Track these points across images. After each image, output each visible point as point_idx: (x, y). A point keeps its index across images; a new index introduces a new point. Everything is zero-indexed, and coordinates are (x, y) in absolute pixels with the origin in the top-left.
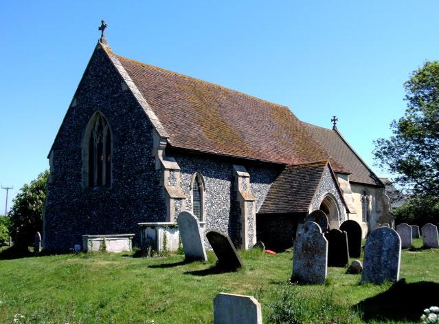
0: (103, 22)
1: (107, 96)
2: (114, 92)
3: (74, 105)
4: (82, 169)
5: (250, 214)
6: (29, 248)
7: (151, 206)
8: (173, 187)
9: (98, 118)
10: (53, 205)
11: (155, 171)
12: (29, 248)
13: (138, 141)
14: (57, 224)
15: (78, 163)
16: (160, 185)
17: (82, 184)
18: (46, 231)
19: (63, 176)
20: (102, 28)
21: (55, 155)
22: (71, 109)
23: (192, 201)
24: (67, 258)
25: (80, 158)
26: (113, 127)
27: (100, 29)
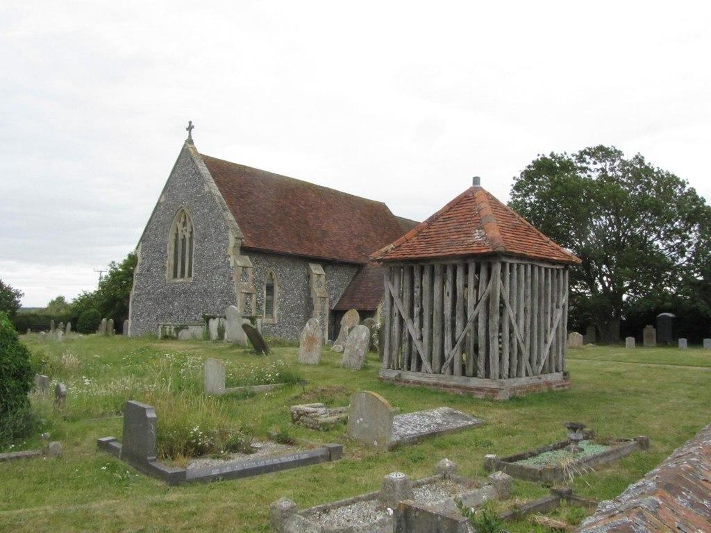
0: (190, 123)
1: (191, 195)
2: (198, 192)
3: (162, 201)
4: (167, 262)
5: (323, 309)
6: (625, 286)
7: (225, 299)
8: (245, 283)
9: (183, 215)
10: (139, 295)
11: (229, 268)
12: (625, 286)
13: (217, 240)
14: (143, 313)
15: (163, 257)
16: (381, 209)
17: (166, 275)
18: (132, 319)
19: (149, 267)
20: (190, 128)
21: (143, 246)
22: (159, 204)
23: (265, 296)
24: (542, 501)
25: (166, 251)
26: (196, 225)
27: (187, 129)
